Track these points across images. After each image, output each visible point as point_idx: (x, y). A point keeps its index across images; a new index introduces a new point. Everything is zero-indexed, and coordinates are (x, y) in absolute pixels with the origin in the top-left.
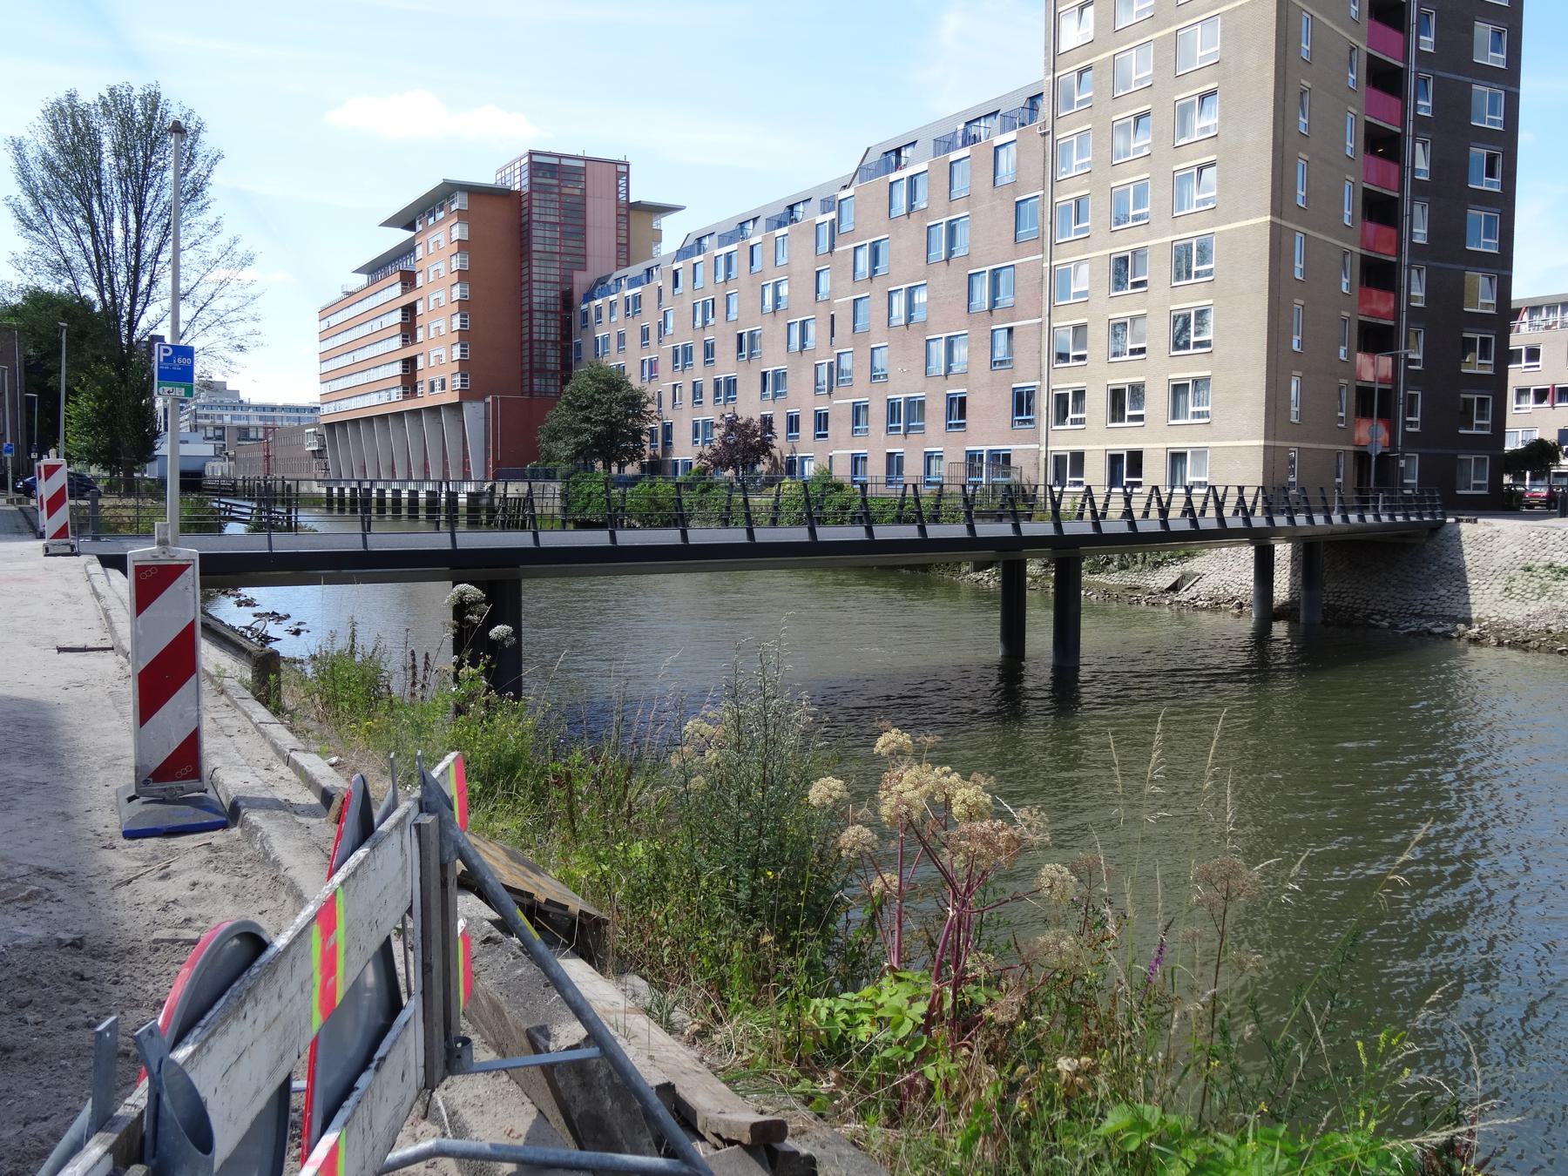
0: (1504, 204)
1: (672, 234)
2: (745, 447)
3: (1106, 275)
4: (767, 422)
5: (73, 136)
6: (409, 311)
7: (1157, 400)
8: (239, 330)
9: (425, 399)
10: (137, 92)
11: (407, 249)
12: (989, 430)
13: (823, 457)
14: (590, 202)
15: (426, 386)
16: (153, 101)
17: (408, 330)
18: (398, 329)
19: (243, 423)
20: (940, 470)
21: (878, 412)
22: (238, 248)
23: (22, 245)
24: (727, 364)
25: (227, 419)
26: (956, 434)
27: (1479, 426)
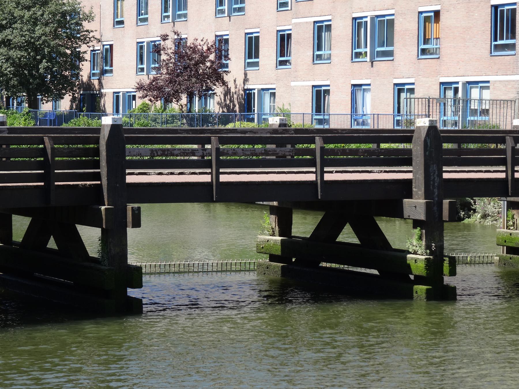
4: (222, 45)
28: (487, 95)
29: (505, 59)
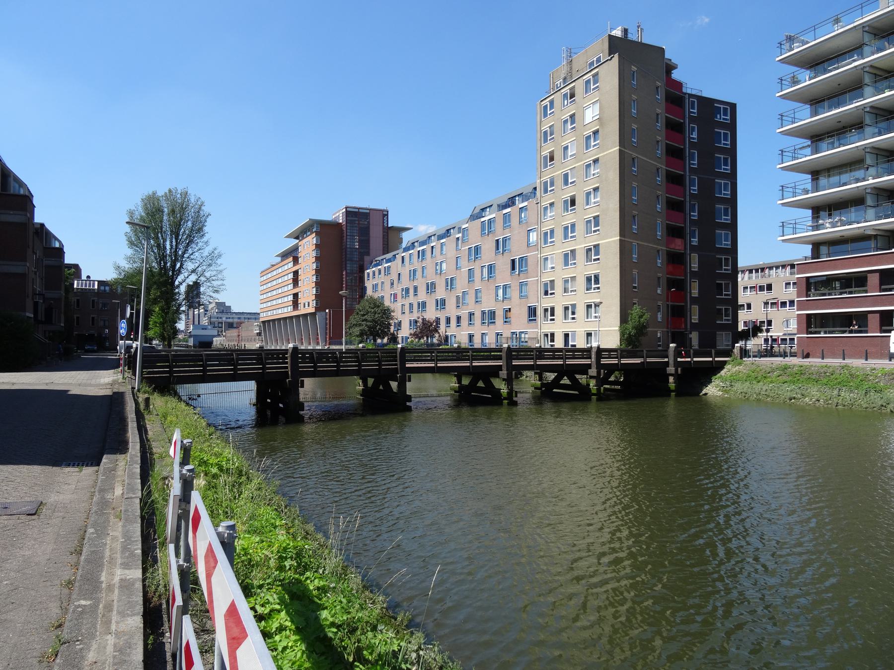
0: (733, 227)
1: (407, 238)
2: (427, 328)
3: (561, 259)
4: (438, 320)
5: (153, 207)
6: (296, 273)
7: (581, 311)
8: (215, 283)
9: (302, 311)
10: (179, 191)
11: (295, 249)
12: (519, 323)
13: (460, 336)
14: (371, 227)
15: (302, 305)
16: (185, 194)
17: (296, 281)
18: (291, 281)
19: (230, 320)
20: (487, 340)
21: (478, 315)
22: (216, 252)
23: (130, 252)
24: (422, 296)
25: (224, 319)
26: (507, 326)
27: (725, 320)
28: (527, 336)
29: (533, 324)
